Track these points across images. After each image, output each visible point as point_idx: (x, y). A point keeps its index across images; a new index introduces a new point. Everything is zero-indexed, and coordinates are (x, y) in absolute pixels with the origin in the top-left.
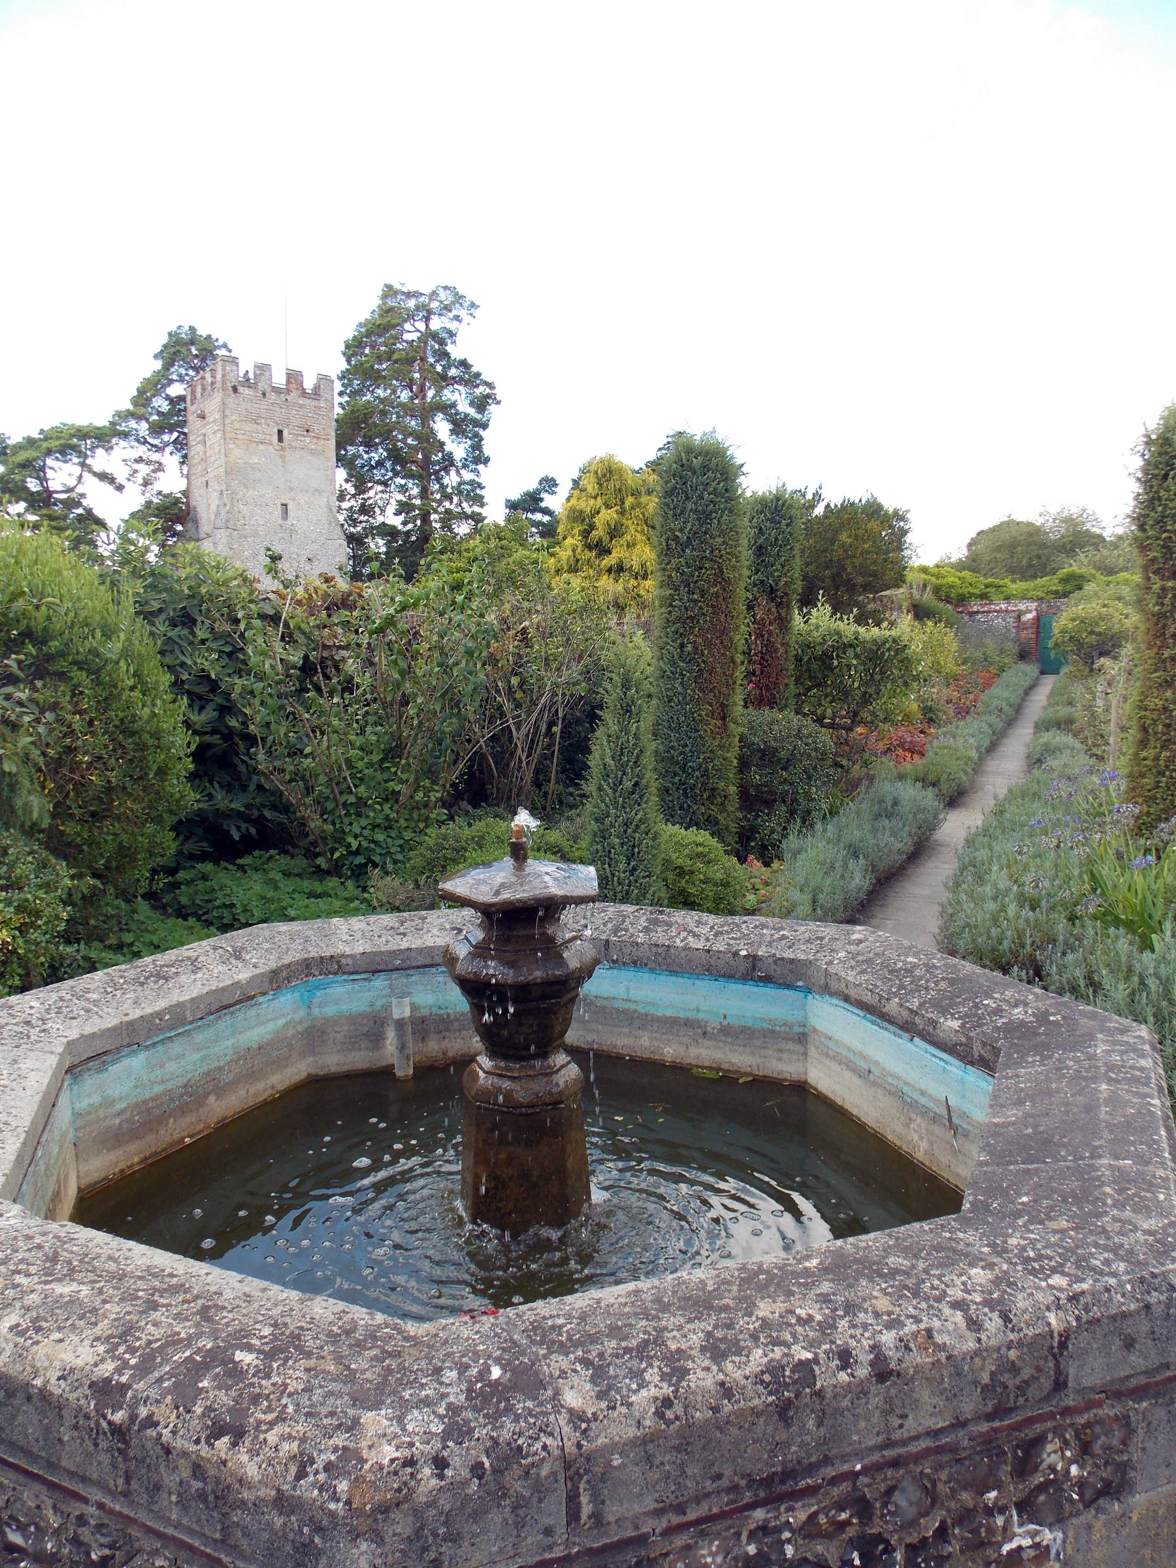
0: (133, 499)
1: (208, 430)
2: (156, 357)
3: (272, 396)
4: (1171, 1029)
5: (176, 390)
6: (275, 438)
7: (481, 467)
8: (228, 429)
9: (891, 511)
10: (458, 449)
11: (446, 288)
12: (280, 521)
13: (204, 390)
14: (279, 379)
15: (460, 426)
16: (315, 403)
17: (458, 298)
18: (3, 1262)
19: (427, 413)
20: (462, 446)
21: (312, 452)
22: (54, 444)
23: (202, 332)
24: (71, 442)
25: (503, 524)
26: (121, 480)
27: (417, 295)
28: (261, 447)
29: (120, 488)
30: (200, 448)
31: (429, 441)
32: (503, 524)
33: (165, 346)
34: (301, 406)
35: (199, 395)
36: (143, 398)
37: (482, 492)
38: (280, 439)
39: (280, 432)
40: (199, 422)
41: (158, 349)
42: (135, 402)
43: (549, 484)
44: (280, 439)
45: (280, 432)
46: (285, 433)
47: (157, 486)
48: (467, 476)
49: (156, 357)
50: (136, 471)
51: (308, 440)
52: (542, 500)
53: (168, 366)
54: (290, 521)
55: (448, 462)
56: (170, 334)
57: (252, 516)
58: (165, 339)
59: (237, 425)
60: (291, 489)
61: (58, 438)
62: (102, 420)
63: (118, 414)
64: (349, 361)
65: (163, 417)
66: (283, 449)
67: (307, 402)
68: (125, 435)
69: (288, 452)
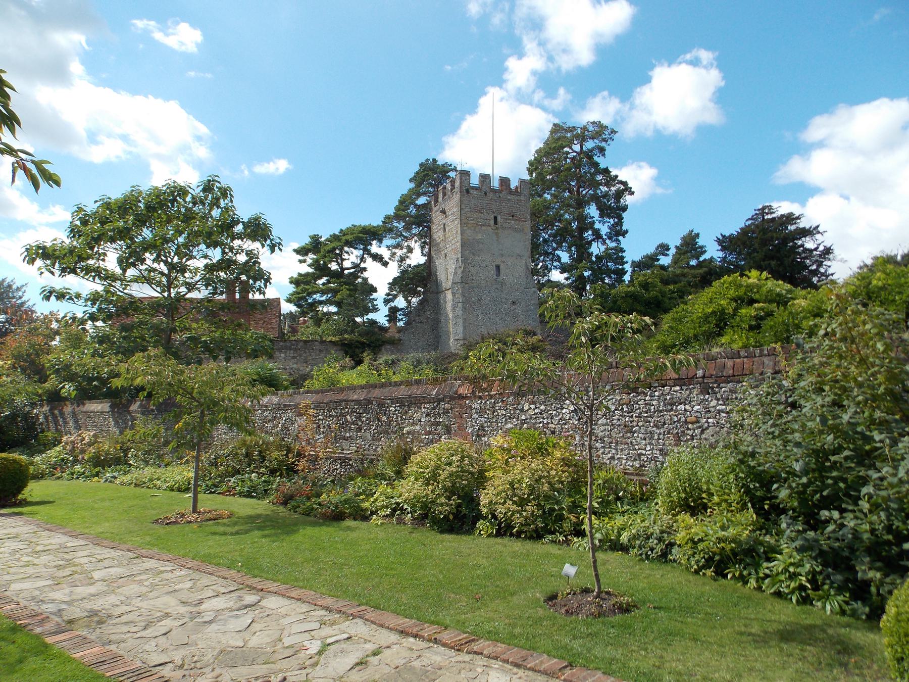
0: (393, 271)
1: (447, 221)
2: (411, 181)
3: (491, 195)
5: (422, 200)
6: (492, 222)
7: (620, 238)
12: (495, 277)
13: (444, 195)
14: (496, 184)
15: (605, 211)
16: (518, 198)
18: (2, 569)
19: (581, 203)
21: (516, 230)
22: (349, 237)
24: (363, 237)
26: (386, 258)
28: (484, 228)
29: (386, 264)
31: (585, 224)
33: (418, 173)
35: (440, 199)
36: (405, 202)
37: (624, 255)
38: (496, 222)
39: (495, 218)
40: (442, 216)
41: (412, 175)
42: (397, 209)
43: (663, 249)
44: (496, 222)
45: (495, 218)
46: (499, 218)
47: (408, 262)
49: (411, 181)
50: (395, 254)
52: (658, 260)
53: (419, 185)
54: (502, 276)
55: (597, 235)
56: (421, 165)
57: (477, 274)
58: (417, 168)
59: (469, 214)
60: (502, 255)
61: (352, 234)
62: (376, 220)
63: (388, 218)
65: (412, 218)
66: (497, 229)
67: (512, 197)
68: (390, 230)
69: (500, 231)
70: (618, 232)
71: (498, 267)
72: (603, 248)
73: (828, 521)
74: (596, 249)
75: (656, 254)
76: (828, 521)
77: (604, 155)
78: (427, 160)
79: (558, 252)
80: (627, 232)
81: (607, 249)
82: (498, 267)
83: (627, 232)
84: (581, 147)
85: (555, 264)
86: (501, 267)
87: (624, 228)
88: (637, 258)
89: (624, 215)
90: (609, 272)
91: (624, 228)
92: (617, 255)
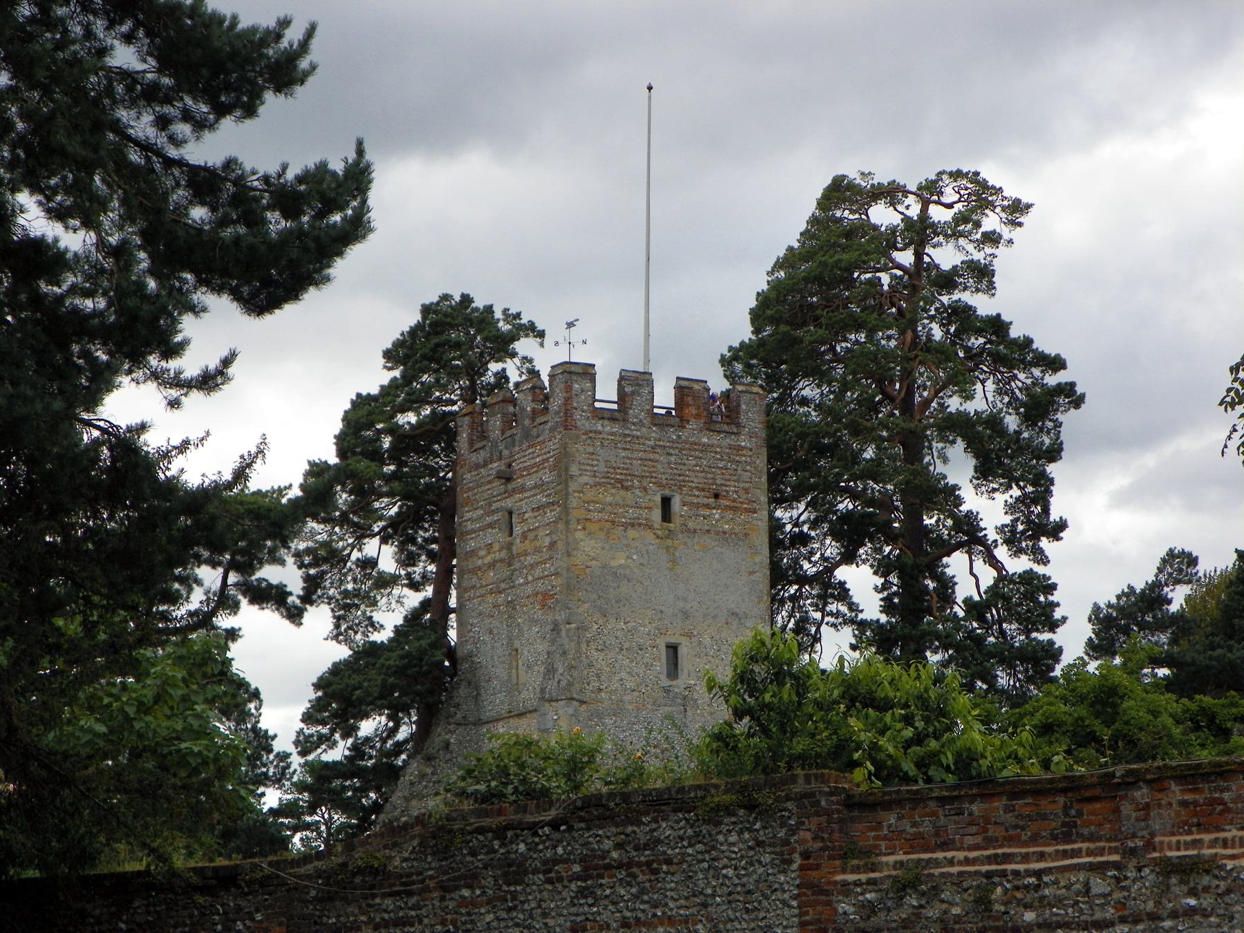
4: (507, 927)
6: (657, 515)
7: (1044, 543)
8: (573, 502)
9: (331, 271)
10: (991, 509)
11: (957, 175)
12: (665, 682)
17: (982, 195)
20: (1001, 498)
23: (736, 344)
25: (333, 459)
27: (891, 193)
28: (632, 533)
29: (295, 615)
30: (496, 536)
32: (333, 459)
34: (705, 448)
38: (667, 516)
39: (666, 502)
44: (667, 516)
45: (666, 502)
48: (1017, 565)
51: (717, 514)
55: (969, 534)
59: (590, 495)
60: (686, 615)
64: (757, 331)
66: (670, 534)
70: (1036, 526)
71: (673, 649)
72: (988, 576)
73: (500, 551)
74: (967, 576)
75: (1155, 586)
76: (500, 551)
77: (991, 287)
78: (446, 297)
79: (842, 573)
80: (1062, 525)
81: (1003, 577)
82: (673, 649)
83: (1062, 525)
84: (919, 255)
85: (832, 607)
86: (682, 651)
87: (1054, 516)
88: (1107, 594)
89: (1052, 469)
90: (1008, 656)
91: (1054, 516)
92: (1030, 600)
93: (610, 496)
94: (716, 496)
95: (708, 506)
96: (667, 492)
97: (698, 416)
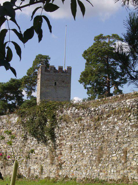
21: (64, 87)
39: (55, 83)
45: (55, 83)
93: (47, 82)
94: (63, 82)
95: (62, 83)
96: (55, 82)
97: (61, 71)
